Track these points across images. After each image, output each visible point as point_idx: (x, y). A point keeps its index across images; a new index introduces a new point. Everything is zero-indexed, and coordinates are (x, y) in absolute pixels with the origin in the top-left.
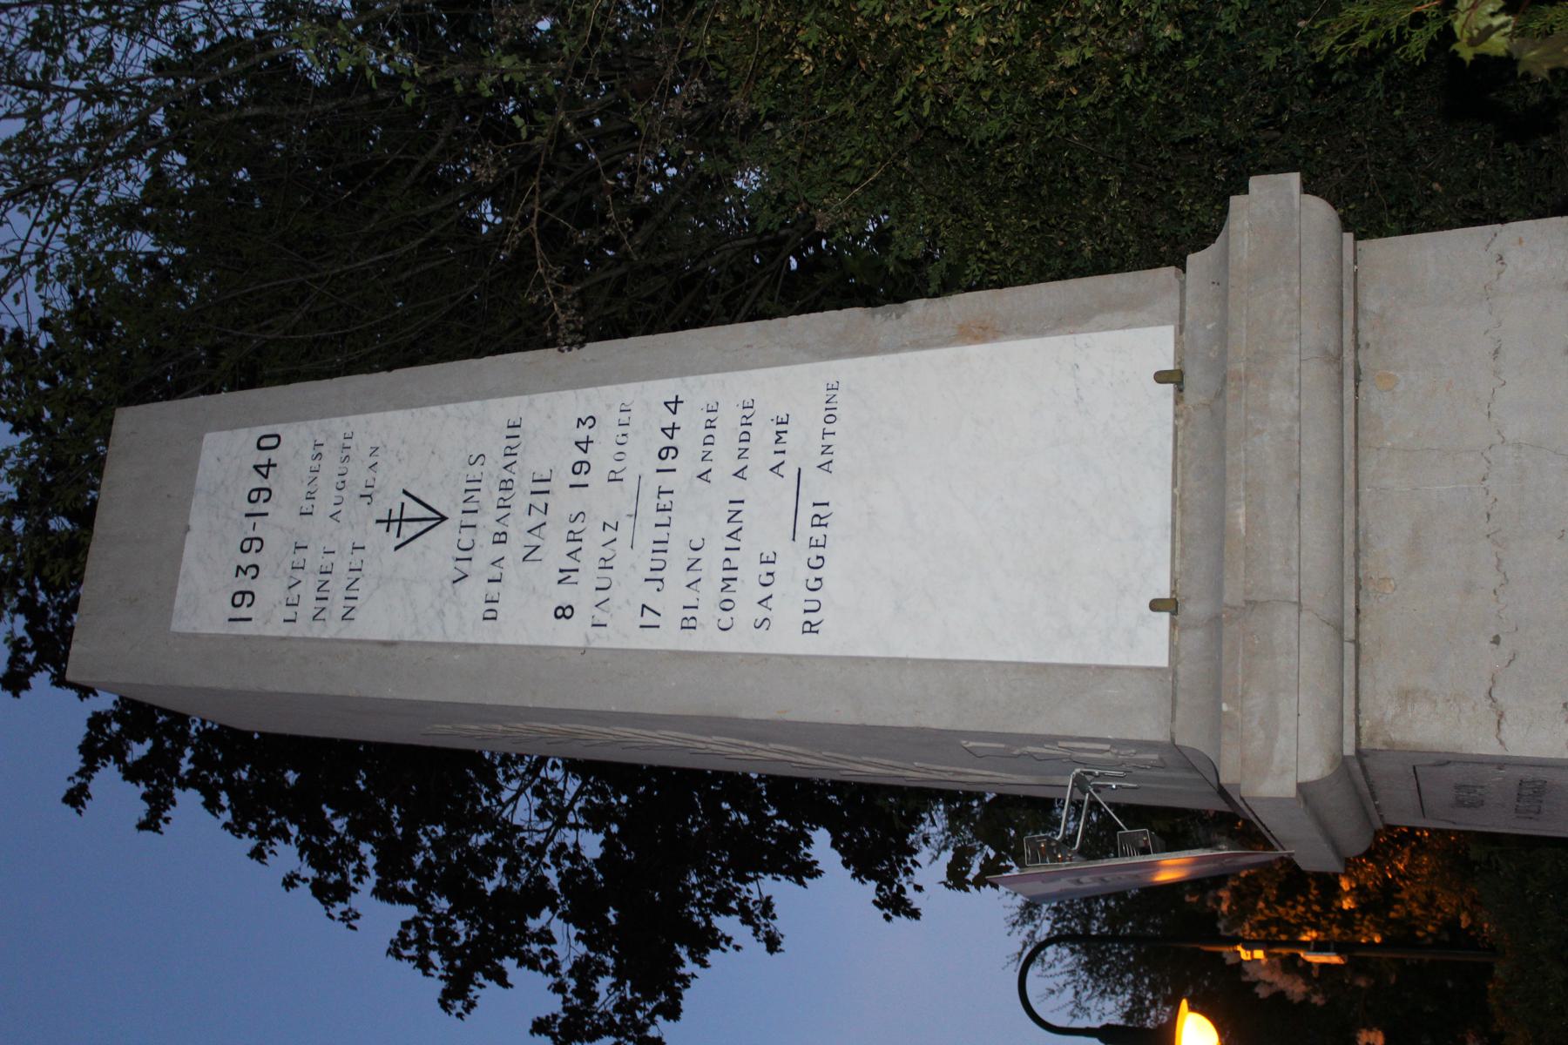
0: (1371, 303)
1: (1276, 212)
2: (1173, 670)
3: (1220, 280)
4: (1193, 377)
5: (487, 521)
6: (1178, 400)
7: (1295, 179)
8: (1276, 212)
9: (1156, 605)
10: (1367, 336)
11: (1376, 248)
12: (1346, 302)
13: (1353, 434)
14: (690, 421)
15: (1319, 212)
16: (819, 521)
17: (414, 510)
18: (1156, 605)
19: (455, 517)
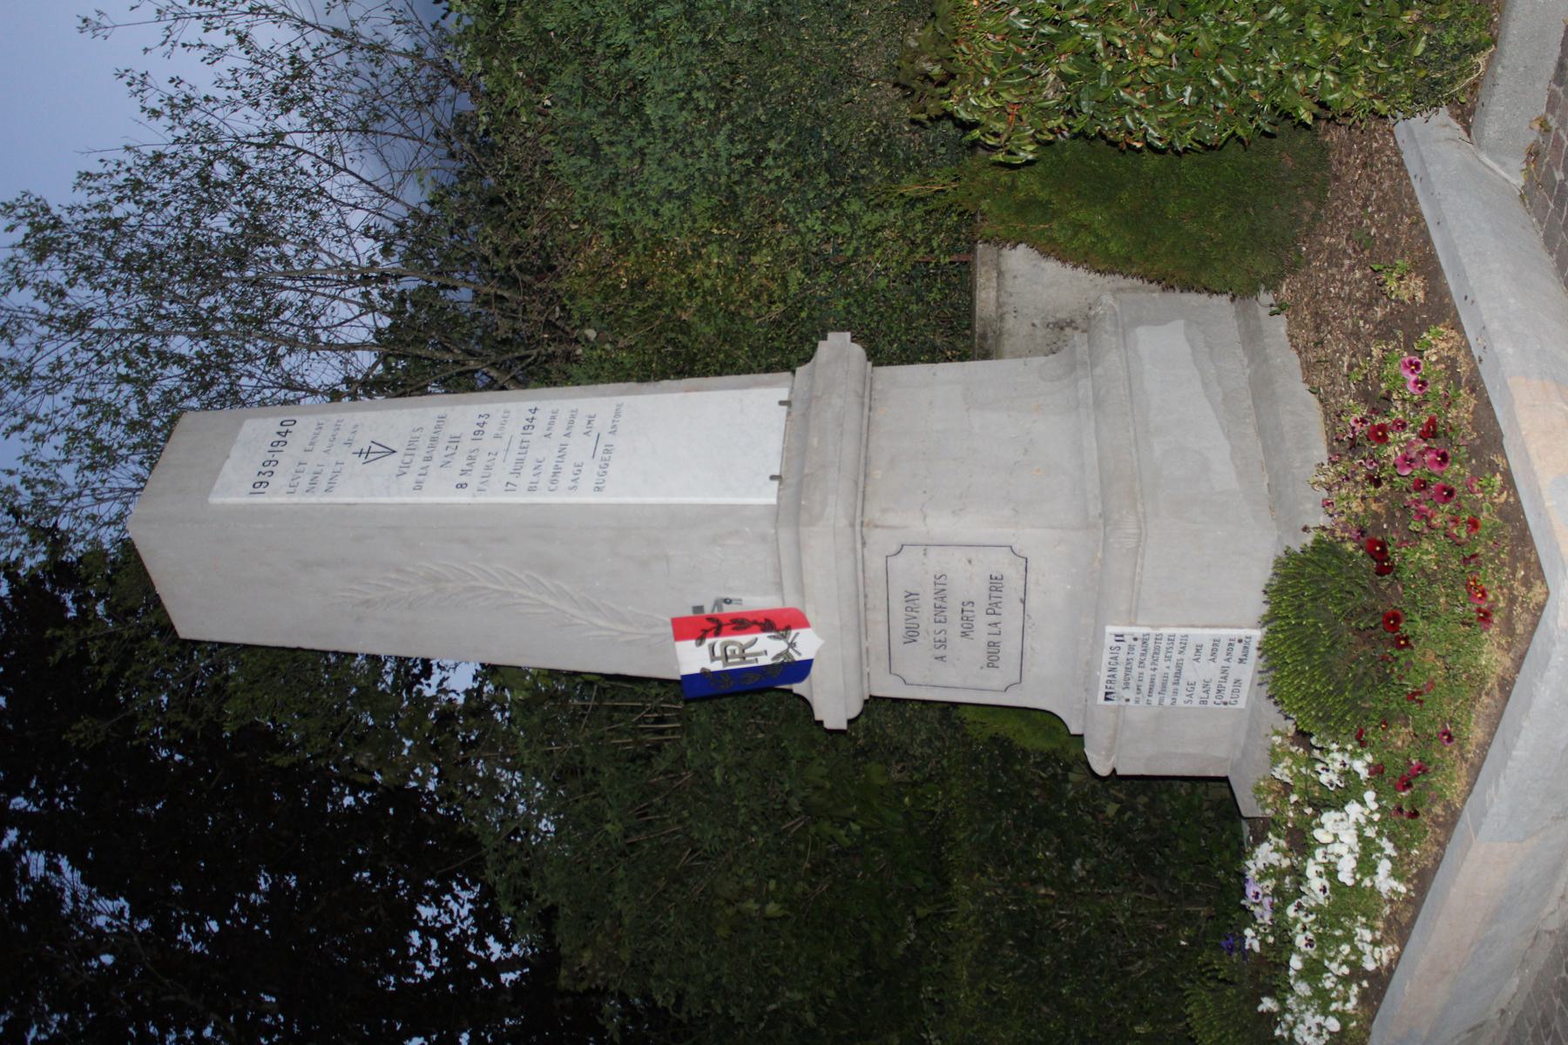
0: (878, 386)
1: (838, 351)
2: (778, 505)
3: (811, 375)
4: (795, 404)
5: (422, 452)
6: (789, 414)
7: (848, 335)
8: (838, 351)
9: (773, 478)
10: (875, 395)
11: (885, 371)
12: (868, 384)
13: (867, 430)
14: (542, 419)
15: (858, 350)
16: (607, 451)
17: (375, 448)
18: (773, 478)
19: (401, 450)
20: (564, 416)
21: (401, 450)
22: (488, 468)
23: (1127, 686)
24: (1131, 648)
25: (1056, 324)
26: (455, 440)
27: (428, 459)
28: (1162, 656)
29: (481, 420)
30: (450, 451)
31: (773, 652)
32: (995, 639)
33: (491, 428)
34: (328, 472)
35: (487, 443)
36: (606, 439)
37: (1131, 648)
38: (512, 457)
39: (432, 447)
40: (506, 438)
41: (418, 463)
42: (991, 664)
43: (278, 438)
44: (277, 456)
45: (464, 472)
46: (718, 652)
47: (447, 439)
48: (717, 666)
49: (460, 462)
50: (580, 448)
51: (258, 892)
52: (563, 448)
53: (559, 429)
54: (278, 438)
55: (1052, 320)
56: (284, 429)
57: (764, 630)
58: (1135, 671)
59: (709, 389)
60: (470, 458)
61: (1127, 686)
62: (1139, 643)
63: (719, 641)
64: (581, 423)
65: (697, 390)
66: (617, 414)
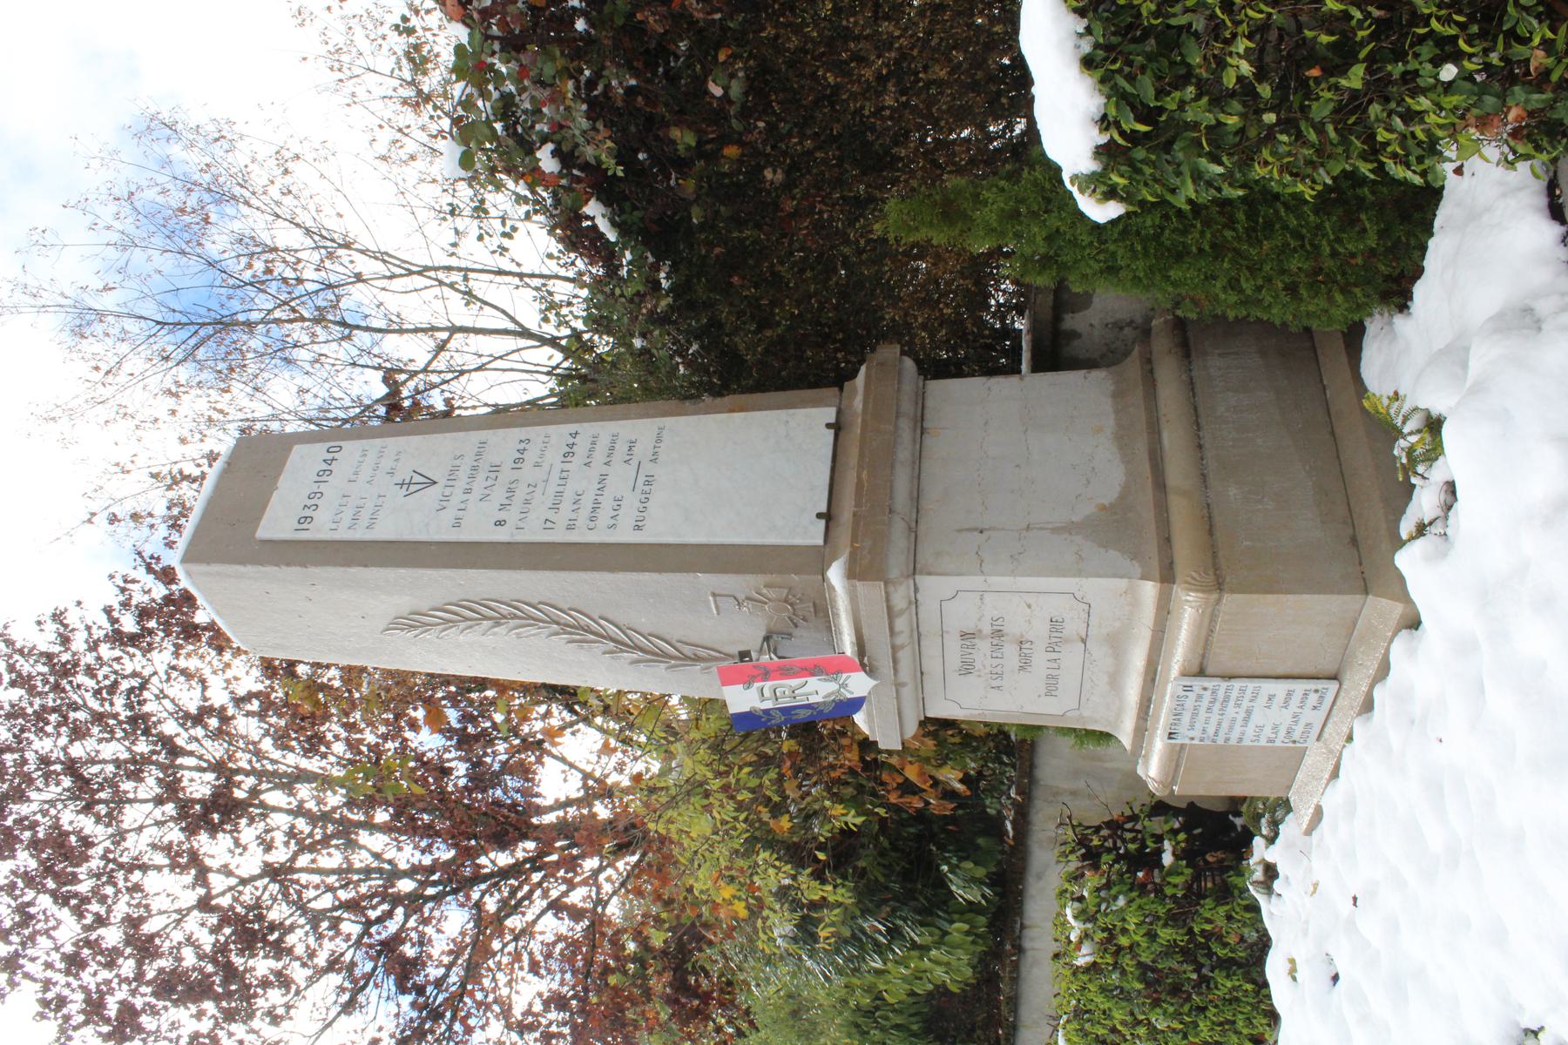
5: (462, 483)
11: (937, 387)
16: (648, 483)
19: (442, 482)
20: (604, 441)
21: (442, 482)
22: (527, 502)
23: (1192, 727)
24: (1200, 697)
25: (1115, 324)
26: (495, 468)
27: (468, 491)
28: (1231, 703)
29: (522, 446)
30: (490, 482)
31: (822, 693)
32: (1055, 673)
33: (531, 457)
34: (370, 506)
35: (528, 473)
36: (648, 468)
37: (1200, 697)
38: (552, 489)
39: (472, 477)
40: (546, 467)
41: (457, 496)
42: (1049, 694)
43: (325, 467)
44: (323, 488)
45: (503, 507)
46: (767, 693)
47: (488, 468)
48: (768, 705)
49: (499, 495)
50: (621, 478)
51: (443, 698)
52: (603, 478)
53: (600, 455)
54: (325, 467)
55: (1110, 320)
56: (330, 456)
57: (812, 675)
58: (1202, 714)
59: (753, 409)
60: (510, 490)
61: (1192, 727)
62: (1208, 693)
63: (768, 685)
64: (622, 448)
65: (742, 410)
66: (659, 440)
